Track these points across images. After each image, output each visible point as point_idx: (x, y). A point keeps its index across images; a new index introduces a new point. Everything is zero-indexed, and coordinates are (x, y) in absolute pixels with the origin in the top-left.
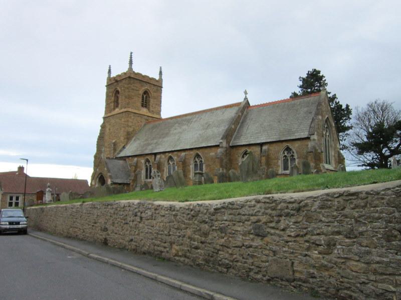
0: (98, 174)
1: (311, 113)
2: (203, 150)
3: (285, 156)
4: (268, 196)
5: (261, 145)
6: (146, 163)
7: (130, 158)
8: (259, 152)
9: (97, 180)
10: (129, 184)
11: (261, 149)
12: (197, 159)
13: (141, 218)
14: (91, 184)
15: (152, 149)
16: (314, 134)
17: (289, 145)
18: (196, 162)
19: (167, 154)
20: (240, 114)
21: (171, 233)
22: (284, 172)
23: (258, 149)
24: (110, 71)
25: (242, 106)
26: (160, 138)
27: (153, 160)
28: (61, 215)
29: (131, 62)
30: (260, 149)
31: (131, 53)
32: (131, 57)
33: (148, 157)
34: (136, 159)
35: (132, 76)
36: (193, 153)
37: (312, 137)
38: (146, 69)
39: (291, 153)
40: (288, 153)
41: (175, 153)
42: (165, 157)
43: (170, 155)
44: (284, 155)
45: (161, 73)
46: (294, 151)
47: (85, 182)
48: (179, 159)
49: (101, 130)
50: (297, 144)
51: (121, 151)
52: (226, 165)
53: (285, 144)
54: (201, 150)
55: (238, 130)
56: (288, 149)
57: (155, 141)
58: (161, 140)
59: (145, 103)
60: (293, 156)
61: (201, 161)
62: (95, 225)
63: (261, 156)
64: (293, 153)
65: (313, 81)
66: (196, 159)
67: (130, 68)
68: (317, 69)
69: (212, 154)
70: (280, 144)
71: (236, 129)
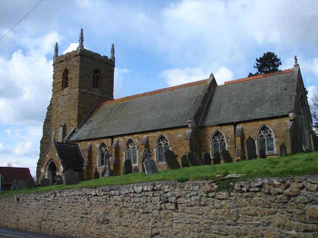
2: (169, 132)
3: (262, 136)
6: (101, 148)
7: (83, 142)
9: (47, 168)
11: (235, 129)
12: (161, 142)
13: (176, 205)
14: (38, 172)
17: (266, 123)
18: (160, 144)
20: (207, 92)
21: (239, 221)
23: (231, 129)
25: (209, 83)
27: (110, 144)
28: (27, 206)
30: (233, 129)
32: (82, 34)
33: (104, 141)
34: (89, 143)
36: (157, 135)
38: (98, 46)
39: (267, 133)
45: (113, 51)
46: (271, 130)
47: (26, 171)
48: (140, 143)
49: (47, 113)
50: (275, 122)
51: (71, 135)
53: (261, 123)
54: (166, 132)
59: (95, 83)
60: (270, 135)
61: (167, 144)
62: (86, 216)
63: (235, 137)
64: (270, 132)
65: (268, 63)
71: (204, 108)
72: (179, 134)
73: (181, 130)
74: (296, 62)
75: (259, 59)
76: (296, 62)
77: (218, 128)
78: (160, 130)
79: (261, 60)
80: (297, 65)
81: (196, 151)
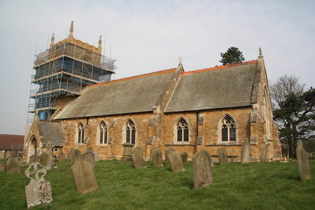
0: (31, 136)
1: (250, 80)
3: (224, 125)
4: (55, 91)
5: (197, 112)
6: (79, 126)
7: (65, 121)
8: (195, 121)
10: (62, 147)
15: (85, 114)
16: (256, 103)
17: (229, 113)
19: (99, 118)
22: (222, 142)
23: (193, 117)
24: (53, 39)
26: (94, 102)
29: (72, 30)
30: (196, 116)
31: (72, 22)
33: (82, 121)
34: (70, 122)
35: (72, 42)
36: (125, 118)
37: (254, 106)
40: (227, 123)
41: (107, 118)
42: (97, 121)
43: (102, 119)
44: (222, 124)
45: (100, 42)
52: (160, 133)
55: (177, 89)
56: (183, 121)
57: (89, 105)
58: (95, 104)
61: (134, 128)
66: (102, 126)
67: (71, 36)
68: (225, 51)
69: (145, 120)
70: (219, 112)
72: (145, 119)
73: (146, 115)
74: (260, 54)
75: (221, 61)
76: (260, 54)
77: (182, 116)
78: (101, 117)
79: (224, 56)
80: (261, 57)
81: (160, 136)
